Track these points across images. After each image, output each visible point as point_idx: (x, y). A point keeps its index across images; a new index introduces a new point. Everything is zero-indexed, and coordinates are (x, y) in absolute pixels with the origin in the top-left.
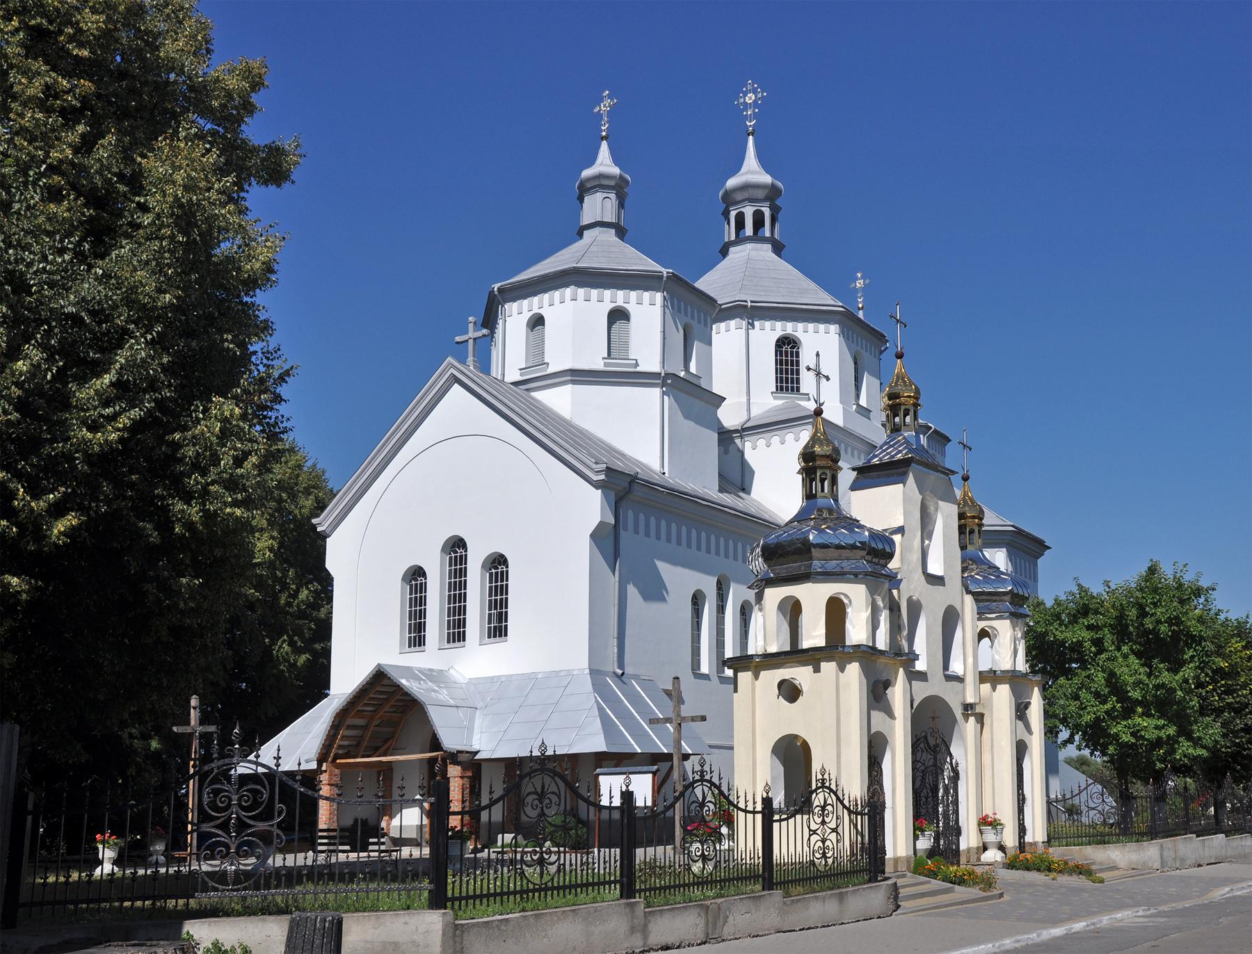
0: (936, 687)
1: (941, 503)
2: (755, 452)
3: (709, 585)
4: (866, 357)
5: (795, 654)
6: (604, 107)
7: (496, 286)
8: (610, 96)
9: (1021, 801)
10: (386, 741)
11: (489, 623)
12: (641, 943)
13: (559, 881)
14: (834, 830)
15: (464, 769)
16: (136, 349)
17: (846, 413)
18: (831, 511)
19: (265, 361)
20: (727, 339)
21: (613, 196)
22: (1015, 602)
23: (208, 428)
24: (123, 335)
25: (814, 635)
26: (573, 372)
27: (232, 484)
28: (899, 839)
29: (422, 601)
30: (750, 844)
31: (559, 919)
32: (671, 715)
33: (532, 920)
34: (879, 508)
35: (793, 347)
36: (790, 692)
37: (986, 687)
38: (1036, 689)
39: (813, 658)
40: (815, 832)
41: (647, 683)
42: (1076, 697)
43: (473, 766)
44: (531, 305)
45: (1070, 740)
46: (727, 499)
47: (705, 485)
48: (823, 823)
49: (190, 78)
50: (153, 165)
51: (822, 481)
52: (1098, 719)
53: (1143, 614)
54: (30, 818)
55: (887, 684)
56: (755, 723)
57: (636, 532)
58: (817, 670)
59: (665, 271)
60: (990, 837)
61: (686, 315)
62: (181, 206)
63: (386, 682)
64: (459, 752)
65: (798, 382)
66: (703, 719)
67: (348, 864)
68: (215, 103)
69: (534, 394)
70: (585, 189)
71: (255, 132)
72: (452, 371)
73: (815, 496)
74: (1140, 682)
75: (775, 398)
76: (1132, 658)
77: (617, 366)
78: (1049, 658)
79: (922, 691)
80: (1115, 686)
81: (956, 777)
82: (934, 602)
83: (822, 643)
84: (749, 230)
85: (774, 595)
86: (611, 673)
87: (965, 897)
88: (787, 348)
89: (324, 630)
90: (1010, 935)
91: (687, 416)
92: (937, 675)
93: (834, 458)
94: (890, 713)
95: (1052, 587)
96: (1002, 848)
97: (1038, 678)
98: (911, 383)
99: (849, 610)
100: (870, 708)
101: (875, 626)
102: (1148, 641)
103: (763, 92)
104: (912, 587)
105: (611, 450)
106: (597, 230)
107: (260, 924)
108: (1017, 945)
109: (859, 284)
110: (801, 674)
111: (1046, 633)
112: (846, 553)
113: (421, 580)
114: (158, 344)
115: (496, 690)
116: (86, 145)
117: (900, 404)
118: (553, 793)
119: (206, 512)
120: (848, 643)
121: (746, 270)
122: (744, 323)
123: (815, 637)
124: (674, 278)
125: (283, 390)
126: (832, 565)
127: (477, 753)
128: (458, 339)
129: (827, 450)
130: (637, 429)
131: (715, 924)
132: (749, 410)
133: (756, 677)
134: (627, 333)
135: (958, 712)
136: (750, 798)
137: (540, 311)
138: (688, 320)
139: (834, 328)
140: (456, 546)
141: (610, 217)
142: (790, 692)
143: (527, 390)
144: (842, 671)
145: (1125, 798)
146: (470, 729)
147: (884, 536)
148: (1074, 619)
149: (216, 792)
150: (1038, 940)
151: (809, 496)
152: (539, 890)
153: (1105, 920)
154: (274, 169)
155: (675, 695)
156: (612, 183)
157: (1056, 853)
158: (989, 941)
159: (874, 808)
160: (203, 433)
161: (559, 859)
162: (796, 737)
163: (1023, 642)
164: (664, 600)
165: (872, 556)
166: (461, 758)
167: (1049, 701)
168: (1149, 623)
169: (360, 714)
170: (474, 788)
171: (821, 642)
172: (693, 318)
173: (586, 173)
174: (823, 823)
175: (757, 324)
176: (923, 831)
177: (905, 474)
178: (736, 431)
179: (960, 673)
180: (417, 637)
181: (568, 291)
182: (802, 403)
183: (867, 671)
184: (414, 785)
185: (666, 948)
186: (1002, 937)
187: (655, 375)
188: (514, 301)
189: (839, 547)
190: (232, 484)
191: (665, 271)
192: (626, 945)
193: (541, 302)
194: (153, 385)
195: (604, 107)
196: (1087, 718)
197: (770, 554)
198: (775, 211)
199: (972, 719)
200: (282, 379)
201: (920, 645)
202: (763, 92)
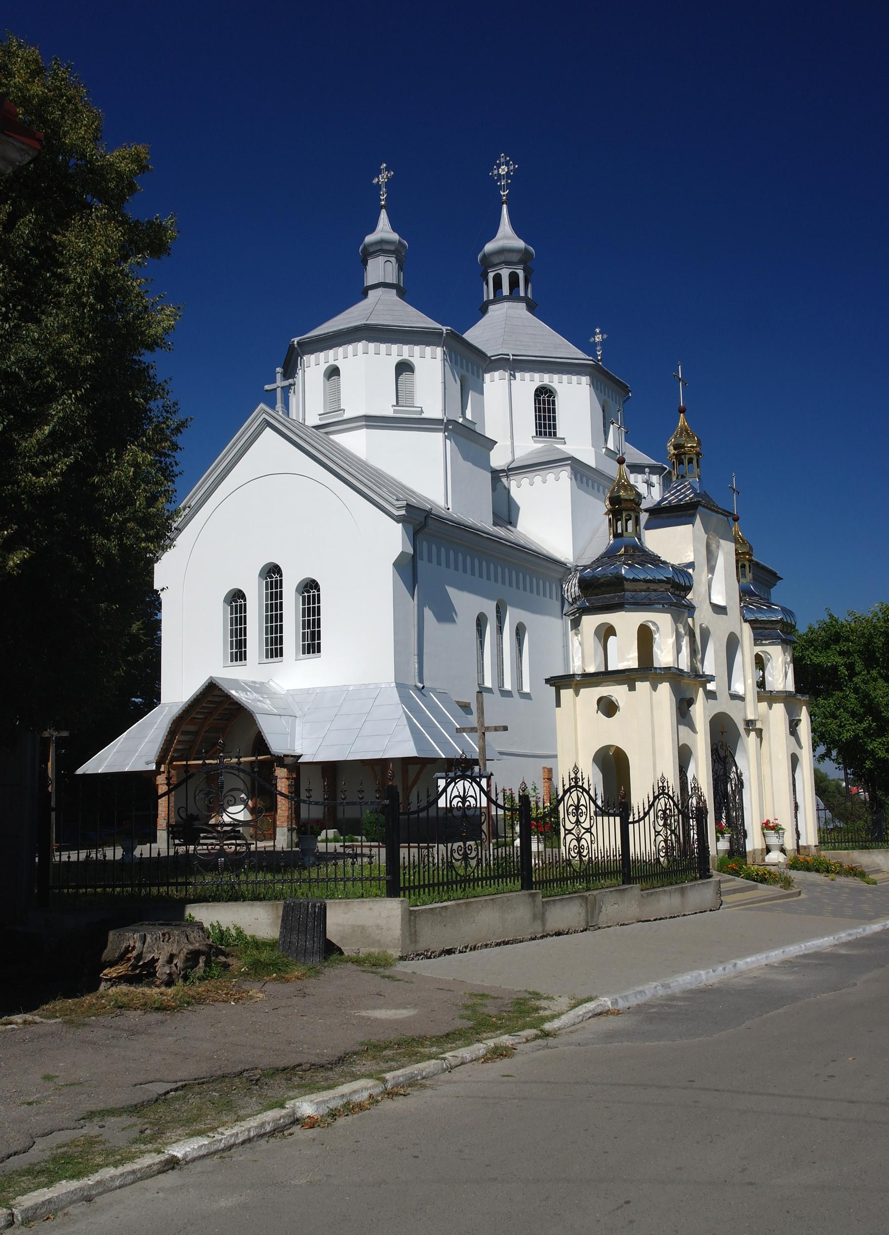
0: (724, 705)
1: (722, 541)
2: (521, 490)
3: (489, 607)
5: (606, 676)
6: (382, 179)
7: (296, 340)
8: (387, 169)
11: (304, 640)
12: (540, 929)
13: (478, 873)
14: (588, 830)
15: (289, 771)
17: (597, 455)
19: (164, 414)
20: (495, 384)
21: (393, 260)
23: (123, 472)
24: (49, 395)
25: (623, 654)
29: (243, 620)
30: (607, 844)
31: (483, 907)
33: (464, 908)
34: (675, 544)
35: (549, 396)
36: (608, 707)
37: (764, 705)
38: (804, 708)
39: (626, 677)
41: (443, 696)
42: (835, 717)
43: (294, 764)
44: (327, 357)
46: (500, 532)
47: (481, 517)
49: (90, 162)
50: (72, 239)
52: (857, 736)
54: (53, 814)
55: (691, 702)
57: (430, 561)
58: (632, 688)
59: (444, 329)
60: (773, 840)
61: (462, 367)
63: (216, 693)
64: (285, 756)
65: (555, 428)
66: (505, 728)
68: (112, 185)
69: (331, 437)
70: (368, 253)
72: (264, 416)
75: (535, 442)
77: (405, 413)
78: (811, 681)
81: (740, 784)
82: (720, 628)
83: (634, 664)
84: (506, 291)
85: (590, 622)
86: (414, 688)
88: (545, 399)
91: (466, 458)
92: (723, 696)
94: (692, 727)
97: (806, 698)
99: (656, 636)
100: (679, 723)
101: (679, 650)
103: (514, 164)
105: (404, 488)
106: (380, 291)
107: (249, 909)
108: (850, 938)
109: (598, 338)
110: (617, 692)
112: (653, 586)
113: (241, 602)
117: (685, 454)
118: (471, 796)
119: (122, 546)
120: (655, 665)
121: (504, 325)
122: (507, 374)
123: (629, 660)
125: (179, 439)
127: (300, 756)
128: (267, 387)
130: (425, 469)
131: (592, 914)
132: (513, 452)
133: (577, 693)
134: (412, 383)
135: (741, 727)
137: (336, 363)
139: (585, 380)
140: (272, 572)
141: (392, 279)
142: (608, 707)
143: (326, 433)
144: (655, 690)
146: (293, 734)
147: (683, 571)
148: (827, 646)
150: (864, 934)
156: (392, 248)
157: (830, 855)
161: (477, 855)
162: (608, 747)
163: (791, 665)
164: (453, 621)
165: (672, 591)
166: (288, 761)
170: (295, 787)
171: (634, 664)
172: (468, 371)
175: (518, 375)
176: (722, 834)
177: (693, 516)
178: (503, 471)
179: (741, 693)
180: (239, 653)
181: (360, 345)
182: (558, 446)
183: (676, 690)
185: (558, 934)
187: (440, 421)
188: (312, 353)
192: (530, 931)
193: (336, 354)
195: (382, 179)
196: (846, 736)
199: (753, 734)
200: (178, 430)
202: (514, 164)
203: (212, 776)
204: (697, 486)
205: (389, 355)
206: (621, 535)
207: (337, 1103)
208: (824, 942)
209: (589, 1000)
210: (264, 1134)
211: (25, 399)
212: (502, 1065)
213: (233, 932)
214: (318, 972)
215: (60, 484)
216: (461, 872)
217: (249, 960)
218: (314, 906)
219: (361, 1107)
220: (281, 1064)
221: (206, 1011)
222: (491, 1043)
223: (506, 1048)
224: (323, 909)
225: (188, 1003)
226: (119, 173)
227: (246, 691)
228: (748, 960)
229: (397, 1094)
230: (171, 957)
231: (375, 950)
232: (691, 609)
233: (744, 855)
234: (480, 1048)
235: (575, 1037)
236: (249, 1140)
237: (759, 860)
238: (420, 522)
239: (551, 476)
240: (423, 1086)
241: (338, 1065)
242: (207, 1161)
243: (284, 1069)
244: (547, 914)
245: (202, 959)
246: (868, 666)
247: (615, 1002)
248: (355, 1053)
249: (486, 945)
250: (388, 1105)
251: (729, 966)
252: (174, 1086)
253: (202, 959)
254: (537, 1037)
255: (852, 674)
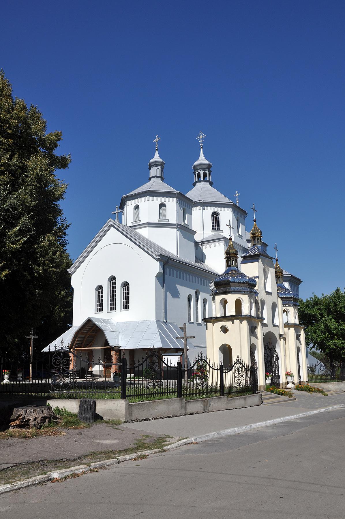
0: (270, 329)
2: (206, 249)
3: (193, 293)
4: (241, 219)
5: (225, 318)
6: (156, 140)
7: (124, 196)
9: (299, 367)
10: (91, 342)
15: (116, 352)
16: (25, 220)
18: (235, 271)
20: (196, 212)
21: (160, 168)
22: (295, 301)
23: (45, 243)
24: (20, 216)
25: (231, 311)
26: (149, 223)
27: (52, 261)
28: (262, 380)
29: (102, 297)
30: (214, 380)
32: (183, 336)
34: (250, 270)
36: (225, 330)
37: (286, 329)
39: (231, 319)
40: (236, 377)
42: (315, 333)
43: (118, 350)
44: (135, 202)
45: (313, 347)
46: (198, 264)
47: (190, 259)
48: (239, 374)
50: (31, 163)
51: (232, 261)
52: (323, 340)
53: (336, 305)
55: (256, 328)
56: (213, 341)
57: (170, 275)
58: (233, 323)
59: (177, 192)
60: (290, 379)
62: (38, 176)
63: (91, 323)
66: (194, 337)
67: (80, 382)
69: (136, 230)
70: (151, 166)
71: (57, 153)
73: (230, 266)
74: (336, 328)
76: (333, 320)
78: (306, 320)
79: (266, 330)
80: (328, 329)
81: (278, 359)
82: (269, 301)
83: (234, 314)
84: (202, 178)
85: (219, 298)
86: (163, 322)
87: (283, 399)
88: (215, 216)
89: (70, 305)
90: (301, 413)
93: (236, 254)
94: (256, 337)
95: (305, 295)
96: (293, 383)
97: (303, 326)
98: (259, 230)
99: (242, 303)
100: (250, 336)
101: (251, 309)
102: (337, 314)
104: (262, 296)
105: (161, 249)
106: (155, 179)
107: (70, 402)
110: (228, 324)
111: (304, 311)
112: (241, 285)
113: (101, 290)
114: (31, 218)
115: (126, 325)
116: (11, 158)
122: (201, 208)
124: (180, 194)
126: (237, 288)
129: (234, 251)
130: (170, 242)
131: (206, 406)
133: (213, 325)
134: (165, 211)
135: (278, 337)
136: (216, 365)
138: (184, 207)
139: (230, 210)
141: (159, 174)
142: (225, 330)
145: (333, 367)
146: (118, 339)
148: (313, 306)
149: (56, 360)
150: (310, 414)
151: (229, 266)
152: (153, 394)
153: (331, 408)
154: (63, 163)
155: (183, 329)
157: (311, 385)
158: (295, 414)
159: (253, 369)
160: (43, 245)
162: (226, 344)
164: (179, 297)
165: (249, 286)
166: (115, 348)
167: (306, 334)
168: (338, 308)
169: (82, 333)
171: (234, 314)
173: (151, 161)
174: (239, 374)
176: (268, 377)
178: (200, 242)
179: (278, 324)
180: (100, 308)
181: (147, 198)
183: (249, 323)
184: (98, 356)
186: (299, 413)
189: (239, 283)
190: (52, 261)
191: (177, 192)
193: (138, 201)
194: (29, 230)
195: (156, 140)
196: (319, 340)
197: (217, 284)
198: (210, 172)
199: (282, 340)
200: (66, 228)
201: (265, 315)
203: (90, 353)
204: (260, 248)
205: (158, 201)
206: (230, 266)
207: (69, 474)
208: (292, 417)
209: (187, 438)
210: (35, 484)
211: (11, 218)
212: (140, 462)
213: (64, 410)
214: (90, 426)
215: (21, 247)
216: (152, 390)
217: (66, 420)
218: (91, 402)
219: (78, 475)
220: (55, 459)
221: (41, 438)
222: (139, 453)
223: (144, 455)
224: (95, 403)
225: (36, 436)
226: (51, 141)
227: (101, 322)
228: (257, 424)
229: (94, 471)
230: (35, 419)
231: (115, 419)
232: (256, 293)
233: (279, 384)
234: (134, 455)
235: (174, 452)
236: (28, 486)
237: (284, 387)
238: (166, 261)
239: (217, 244)
240: (106, 468)
241: (78, 460)
242: (9, 494)
243: (56, 461)
244: (187, 407)
245: (47, 420)
246: (328, 314)
247: (196, 439)
248: (86, 456)
249: (161, 418)
250: (90, 475)
251: (248, 426)
252: (12, 465)
253: (47, 420)
254: (160, 452)
255: (322, 317)
